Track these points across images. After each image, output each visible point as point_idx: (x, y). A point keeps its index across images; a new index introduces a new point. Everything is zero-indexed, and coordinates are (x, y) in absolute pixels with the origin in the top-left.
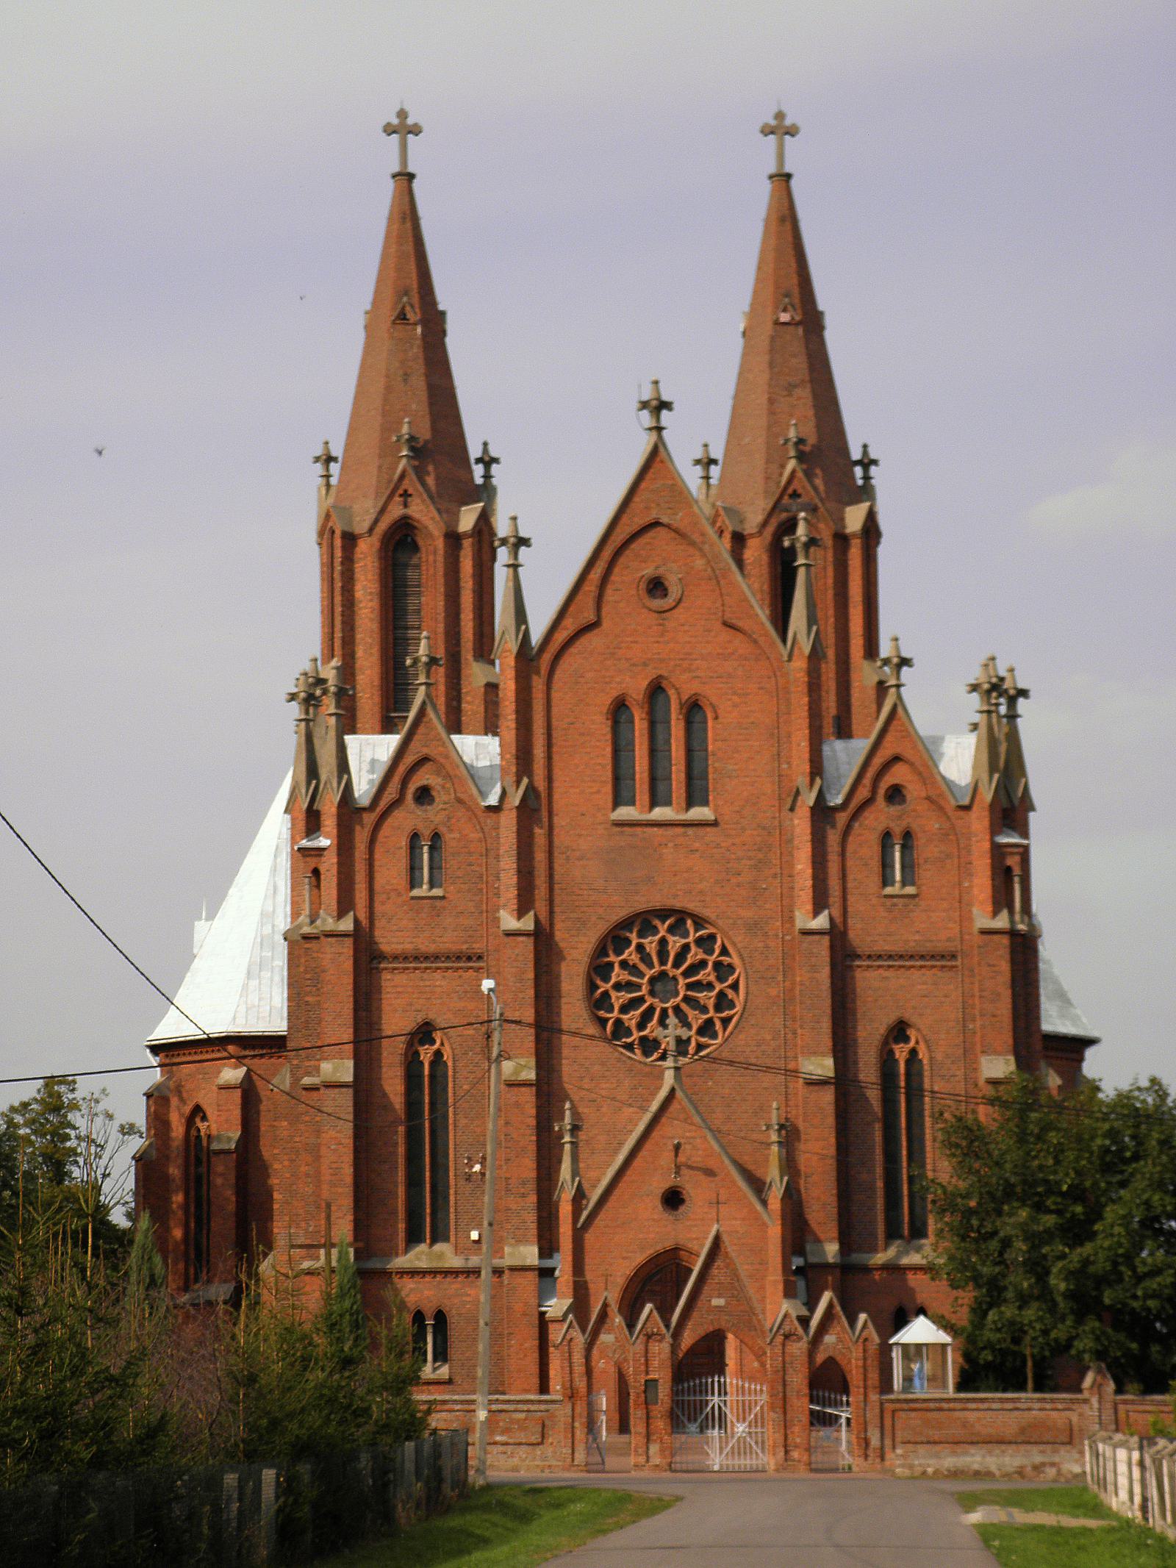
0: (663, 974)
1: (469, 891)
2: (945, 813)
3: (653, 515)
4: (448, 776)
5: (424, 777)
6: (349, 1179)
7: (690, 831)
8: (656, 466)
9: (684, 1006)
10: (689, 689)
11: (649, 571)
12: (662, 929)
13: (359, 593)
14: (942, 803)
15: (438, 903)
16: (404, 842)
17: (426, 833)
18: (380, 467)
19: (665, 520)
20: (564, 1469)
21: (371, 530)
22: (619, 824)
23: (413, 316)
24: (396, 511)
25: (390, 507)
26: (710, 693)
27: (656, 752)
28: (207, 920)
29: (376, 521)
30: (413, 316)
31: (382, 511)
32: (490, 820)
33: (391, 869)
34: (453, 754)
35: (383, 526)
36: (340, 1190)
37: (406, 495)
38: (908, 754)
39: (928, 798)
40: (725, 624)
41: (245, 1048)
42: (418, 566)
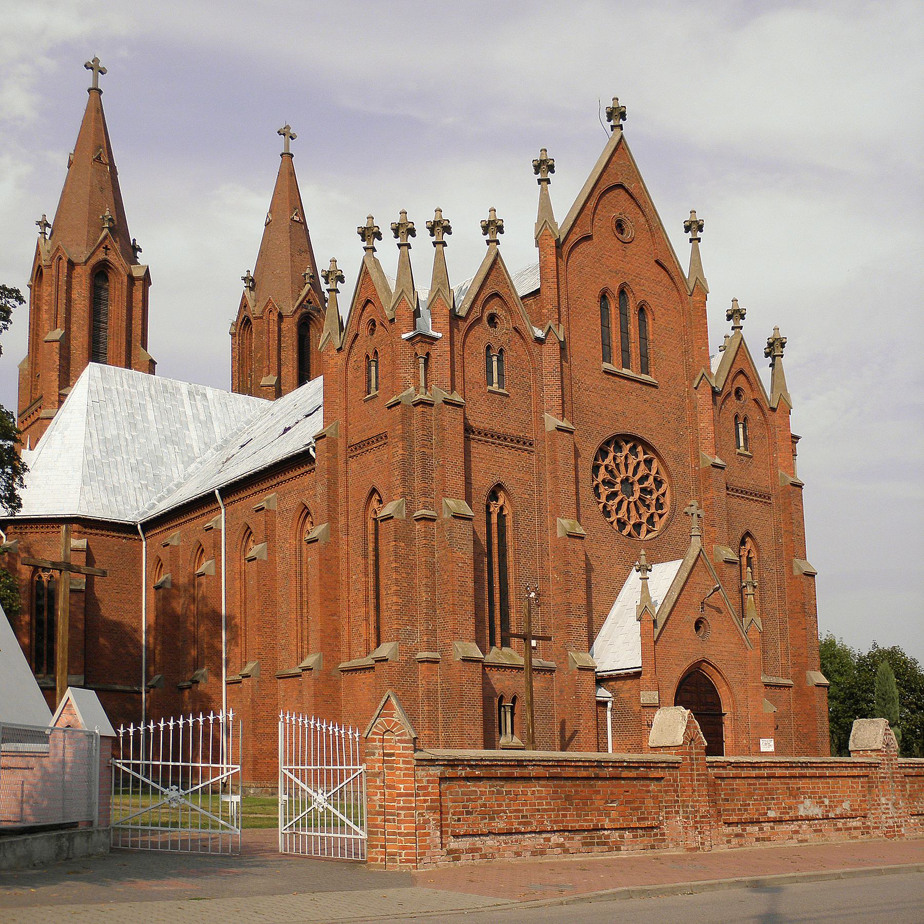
0: (627, 479)
1: (523, 395)
2: (762, 411)
3: (620, 180)
4: (510, 311)
5: (494, 307)
6: (471, 591)
7: (644, 388)
8: (620, 151)
9: (639, 503)
10: (641, 297)
11: (615, 214)
12: (627, 448)
13: (75, 295)
14: (762, 404)
15: (505, 400)
16: (483, 350)
17: (496, 348)
18: (88, 232)
19: (626, 185)
20: (371, 807)
21: (86, 262)
22: (606, 372)
23: (95, 161)
24: (100, 255)
25: (97, 253)
26: (652, 302)
27: (625, 332)
28: (31, 449)
29: (89, 258)
30: (95, 161)
31: (93, 253)
32: (536, 348)
33: (475, 369)
34: (236, 368)
35: (93, 261)
36: (466, 599)
37: (106, 248)
38: (746, 371)
39: (755, 400)
40: (657, 262)
41: (85, 528)
42: (107, 290)
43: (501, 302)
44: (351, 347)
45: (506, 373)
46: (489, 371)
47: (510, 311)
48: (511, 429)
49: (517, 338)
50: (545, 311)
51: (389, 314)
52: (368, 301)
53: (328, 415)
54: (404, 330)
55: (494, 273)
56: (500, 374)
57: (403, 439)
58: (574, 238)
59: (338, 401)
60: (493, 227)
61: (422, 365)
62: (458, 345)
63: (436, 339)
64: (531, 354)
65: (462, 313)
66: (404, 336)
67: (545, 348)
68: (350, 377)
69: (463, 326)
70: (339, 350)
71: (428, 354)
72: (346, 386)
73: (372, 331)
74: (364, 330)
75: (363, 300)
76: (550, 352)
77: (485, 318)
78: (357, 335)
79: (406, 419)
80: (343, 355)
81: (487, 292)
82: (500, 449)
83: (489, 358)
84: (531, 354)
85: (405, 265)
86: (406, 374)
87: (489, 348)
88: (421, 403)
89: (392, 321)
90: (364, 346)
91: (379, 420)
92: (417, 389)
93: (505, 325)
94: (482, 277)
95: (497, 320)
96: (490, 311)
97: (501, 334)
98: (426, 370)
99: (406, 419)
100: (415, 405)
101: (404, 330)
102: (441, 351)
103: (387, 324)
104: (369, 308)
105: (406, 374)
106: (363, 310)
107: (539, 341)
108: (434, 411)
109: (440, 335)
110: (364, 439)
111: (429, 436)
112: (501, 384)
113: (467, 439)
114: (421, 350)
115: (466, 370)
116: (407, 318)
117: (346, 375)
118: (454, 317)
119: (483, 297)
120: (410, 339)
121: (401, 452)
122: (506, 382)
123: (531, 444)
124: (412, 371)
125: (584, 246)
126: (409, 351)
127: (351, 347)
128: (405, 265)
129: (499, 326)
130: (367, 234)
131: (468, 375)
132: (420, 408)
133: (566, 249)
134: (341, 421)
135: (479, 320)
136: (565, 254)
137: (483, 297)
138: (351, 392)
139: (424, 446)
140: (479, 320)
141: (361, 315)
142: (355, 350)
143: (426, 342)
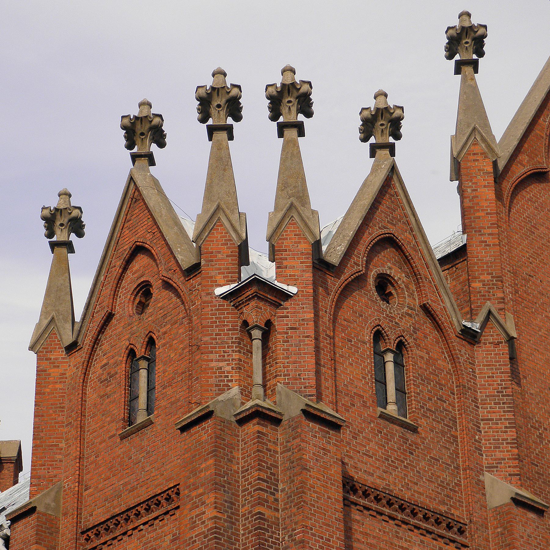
4: (414, 274)
16: (368, 337)
32: (462, 349)
33: (355, 370)
43: (397, 257)
44: (96, 341)
45: (410, 388)
46: (382, 382)
47: (414, 274)
48: (423, 494)
49: (428, 326)
50: (476, 285)
51: (186, 259)
52: (139, 250)
53: (42, 472)
54: (220, 279)
55: (386, 203)
56: (400, 390)
57: (217, 486)
58: (520, 170)
59: (63, 445)
60: (382, 125)
61: (257, 344)
62: (326, 318)
63: (286, 296)
64: (453, 359)
65: (334, 259)
66: (219, 291)
67: (482, 353)
68: (92, 396)
69: (335, 284)
70: (72, 348)
71: (269, 323)
72: (83, 415)
73: (142, 307)
74: (125, 305)
75: (126, 248)
76: (489, 359)
77: (371, 280)
78: (110, 317)
79: (221, 449)
80: (80, 356)
81: (374, 233)
82: (403, 531)
83: (379, 355)
84: (453, 359)
85: (220, 168)
86: (221, 361)
87: (378, 336)
88: (258, 414)
89: (194, 270)
90: (126, 332)
91: (161, 458)
92: (246, 393)
93: (405, 301)
94: (367, 201)
95: (390, 289)
96: (381, 270)
97: (400, 314)
98: (264, 357)
99: (221, 449)
100: (242, 421)
101: (220, 279)
102: (295, 322)
103: (178, 280)
104: (141, 261)
105: (221, 361)
106: (125, 269)
107: (470, 337)
108: (281, 434)
109: (293, 290)
110: (117, 511)
111: (271, 482)
112: (401, 402)
113: (347, 503)
114: (255, 313)
115: (340, 369)
116: (225, 256)
117: (84, 394)
118: (321, 266)
119: (367, 239)
120: (226, 297)
121: (210, 513)
122: (413, 405)
123: (461, 532)
124: (236, 356)
125: (535, 190)
126: (230, 318)
127: (96, 341)
128: (220, 168)
129: (395, 300)
130: (139, 128)
131: (344, 379)
132: (253, 427)
133: (508, 186)
134: (68, 482)
135: (359, 280)
136: (506, 194)
137: (367, 239)
138: (91, 424)
139: (261, 502)
140: (359, 280)
141: (120, 279)
142: (105, 345)
143: (265, 300)
